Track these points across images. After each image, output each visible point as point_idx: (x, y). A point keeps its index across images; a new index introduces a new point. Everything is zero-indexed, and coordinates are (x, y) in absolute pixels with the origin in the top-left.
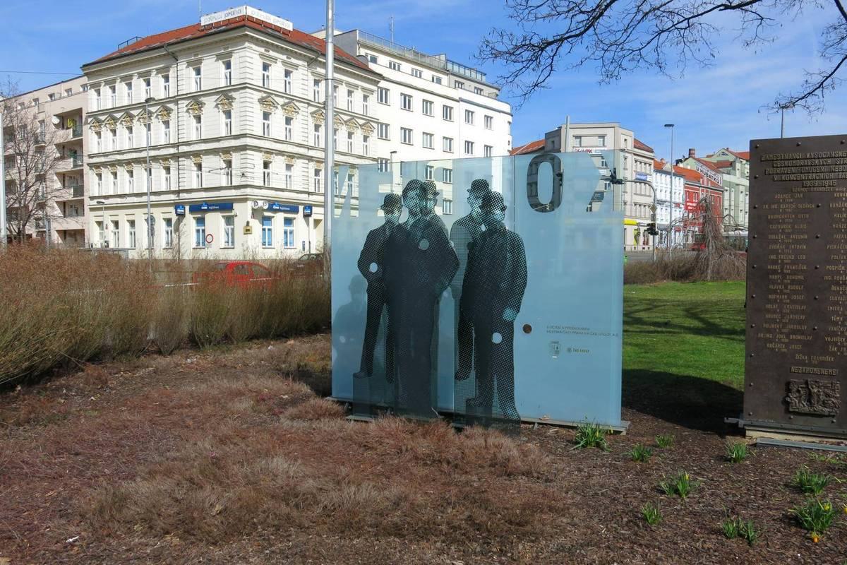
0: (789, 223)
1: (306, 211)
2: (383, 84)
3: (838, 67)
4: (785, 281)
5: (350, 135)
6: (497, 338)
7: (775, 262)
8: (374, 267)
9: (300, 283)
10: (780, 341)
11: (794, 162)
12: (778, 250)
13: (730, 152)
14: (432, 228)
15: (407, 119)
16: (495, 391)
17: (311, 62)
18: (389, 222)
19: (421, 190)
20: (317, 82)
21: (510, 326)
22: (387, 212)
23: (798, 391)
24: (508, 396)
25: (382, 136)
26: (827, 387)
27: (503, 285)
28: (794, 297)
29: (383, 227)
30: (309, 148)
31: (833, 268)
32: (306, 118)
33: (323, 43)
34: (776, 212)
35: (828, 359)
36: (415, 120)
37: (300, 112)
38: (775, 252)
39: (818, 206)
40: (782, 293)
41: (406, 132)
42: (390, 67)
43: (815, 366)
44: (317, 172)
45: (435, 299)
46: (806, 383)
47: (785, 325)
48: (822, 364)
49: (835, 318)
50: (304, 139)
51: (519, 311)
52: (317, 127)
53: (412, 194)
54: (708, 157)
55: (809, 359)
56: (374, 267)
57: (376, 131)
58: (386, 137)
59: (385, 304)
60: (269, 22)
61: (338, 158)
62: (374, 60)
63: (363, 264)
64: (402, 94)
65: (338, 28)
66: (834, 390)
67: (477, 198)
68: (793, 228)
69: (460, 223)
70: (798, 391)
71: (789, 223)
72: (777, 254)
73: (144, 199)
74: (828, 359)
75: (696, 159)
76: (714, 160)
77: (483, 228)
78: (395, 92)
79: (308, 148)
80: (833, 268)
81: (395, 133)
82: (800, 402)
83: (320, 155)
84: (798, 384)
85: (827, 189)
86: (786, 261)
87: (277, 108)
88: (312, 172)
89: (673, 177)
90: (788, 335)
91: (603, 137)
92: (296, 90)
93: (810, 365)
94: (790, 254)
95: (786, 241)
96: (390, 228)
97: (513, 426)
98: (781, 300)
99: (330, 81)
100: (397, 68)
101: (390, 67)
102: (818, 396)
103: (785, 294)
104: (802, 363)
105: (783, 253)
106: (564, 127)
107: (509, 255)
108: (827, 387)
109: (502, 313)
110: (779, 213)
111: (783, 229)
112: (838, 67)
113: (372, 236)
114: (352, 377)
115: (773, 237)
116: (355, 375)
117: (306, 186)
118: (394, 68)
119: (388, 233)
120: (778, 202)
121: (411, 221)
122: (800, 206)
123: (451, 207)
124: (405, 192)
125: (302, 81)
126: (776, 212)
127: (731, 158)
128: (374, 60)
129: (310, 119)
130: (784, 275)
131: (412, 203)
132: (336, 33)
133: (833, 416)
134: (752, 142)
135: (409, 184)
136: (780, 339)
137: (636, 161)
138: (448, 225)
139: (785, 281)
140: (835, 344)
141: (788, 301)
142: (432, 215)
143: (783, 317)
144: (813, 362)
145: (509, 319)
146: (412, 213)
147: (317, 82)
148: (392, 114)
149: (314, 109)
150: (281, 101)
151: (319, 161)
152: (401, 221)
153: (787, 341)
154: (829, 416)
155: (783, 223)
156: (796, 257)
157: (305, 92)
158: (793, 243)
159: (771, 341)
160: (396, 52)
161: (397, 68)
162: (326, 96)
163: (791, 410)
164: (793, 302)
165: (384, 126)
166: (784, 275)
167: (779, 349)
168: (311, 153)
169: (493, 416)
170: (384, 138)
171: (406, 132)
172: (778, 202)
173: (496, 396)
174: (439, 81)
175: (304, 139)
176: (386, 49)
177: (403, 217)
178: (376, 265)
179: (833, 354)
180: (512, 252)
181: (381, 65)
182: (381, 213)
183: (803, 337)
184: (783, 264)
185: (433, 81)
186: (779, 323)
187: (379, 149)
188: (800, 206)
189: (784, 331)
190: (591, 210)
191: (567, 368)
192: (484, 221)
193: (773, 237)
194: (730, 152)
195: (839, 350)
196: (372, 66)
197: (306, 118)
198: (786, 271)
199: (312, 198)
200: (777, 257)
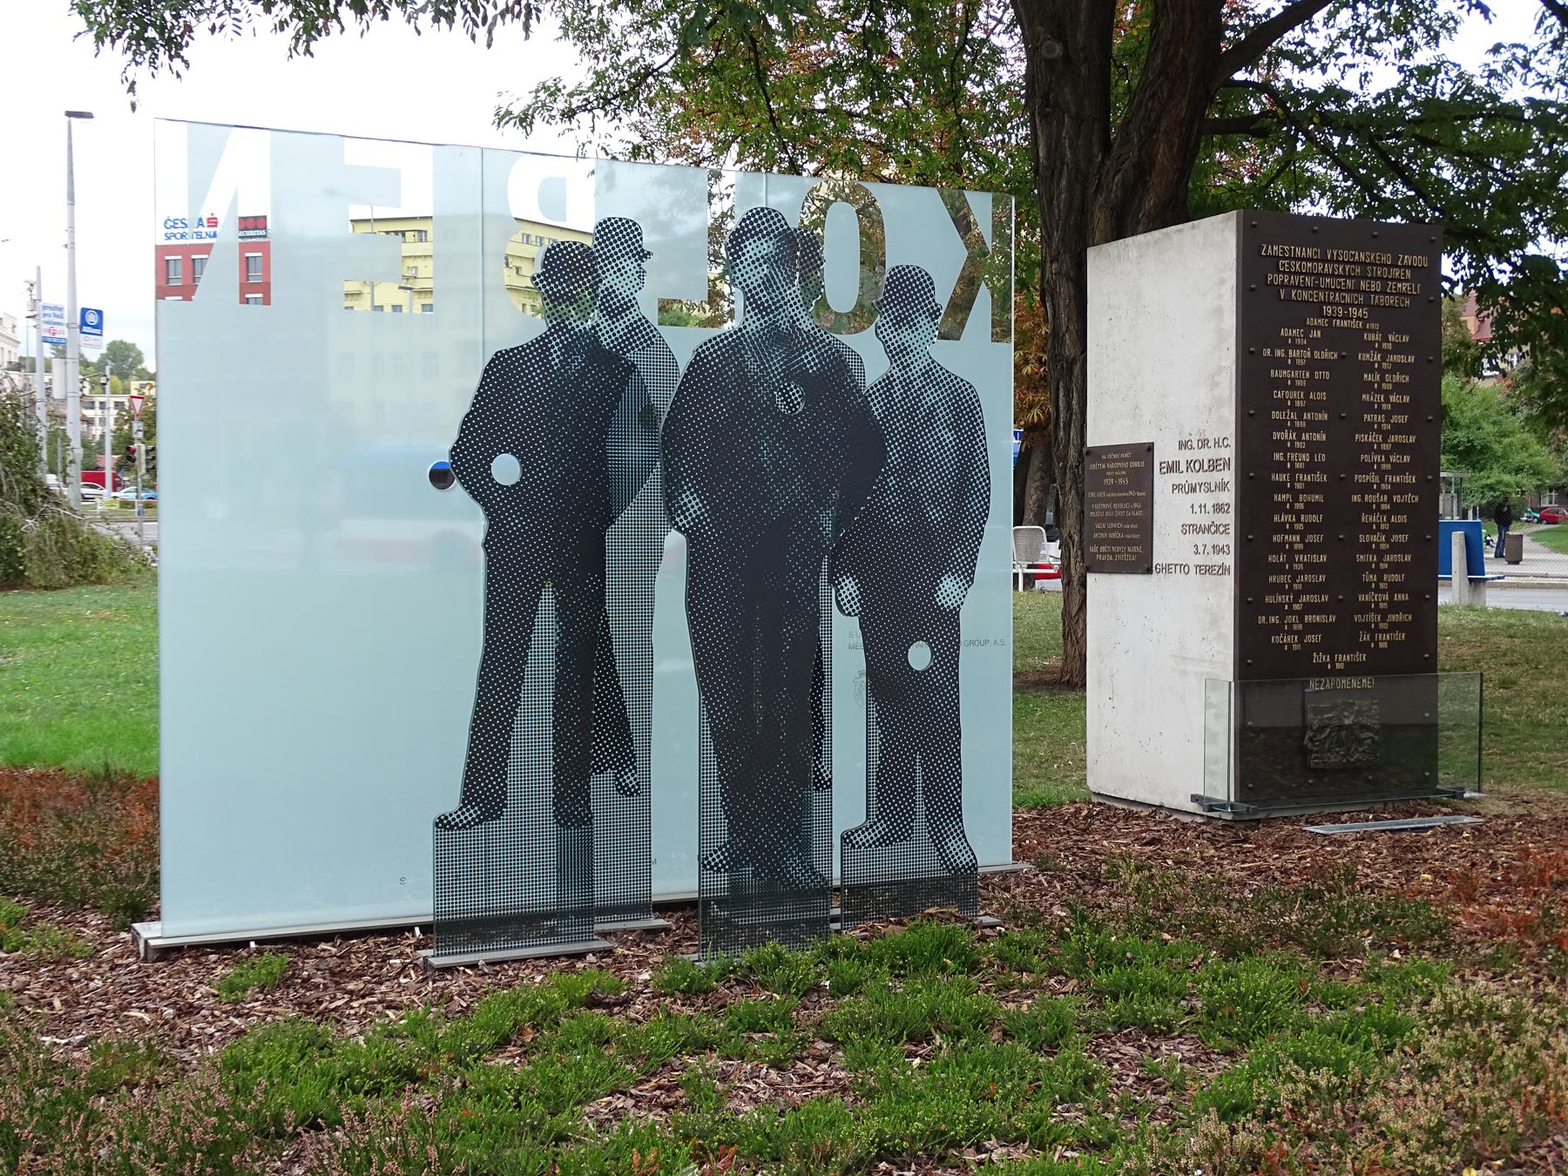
3: (71, 173)
8: (506, 470)
9: (515, 524)
10: (1291, 632)
12: (1285, 442)
28: (1310, 538)
34: (1281, 364)
38: (1281, 446)
56: (506, 470)
95: (1298, 424)
110: (1286, 367)
112: (71, 173)
113: (503, 372)
114: (429, 831)
116: (442, 824)
120: (1284, 344)
122: (1317, 355)
142: (631, 317)
145: (949, 603)
156: (1312, 457)
166: (1295, 494)
167: (1290, 645)
172: (1284, 344)
178: (508, 456)
179: (1364, 647)
180: (955, 427)
184: (1293, 471)
188: (1317, 355)
189: (1297, 607)
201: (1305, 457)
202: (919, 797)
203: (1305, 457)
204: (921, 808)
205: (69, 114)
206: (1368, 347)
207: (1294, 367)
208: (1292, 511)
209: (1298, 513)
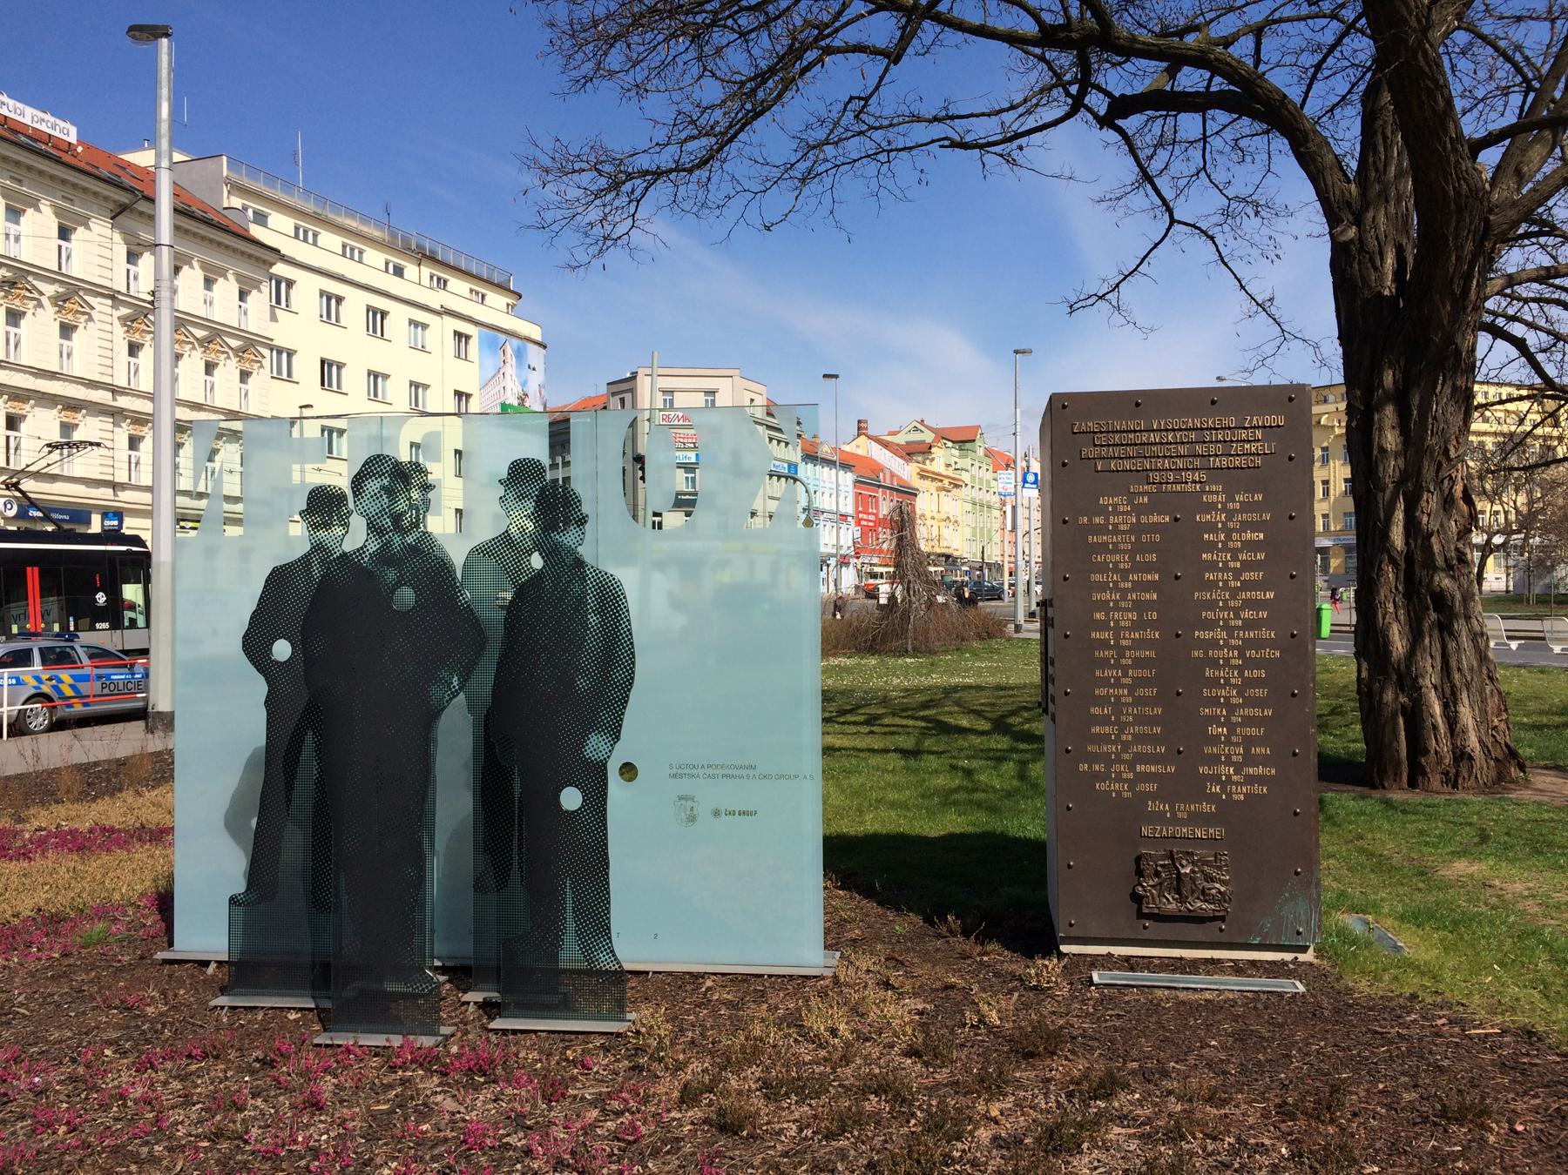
0: (1125, 552)
1: (107, 523)
2: (280, 269)
4: (1123, 661)
5: (210, 368)
6: (571, 799)
7: (1102, 626)
8: (282, 650)
10: (1119, 779)
11: (1131, 436)
13: (928, 428)
14: (427, 565)
15: (333, 343)
16: (569, 915)
17: (118, 213)
18: (318, 547)
19: (394, 479)
20: (132, 257)
21: (600, 769)
22: (314, 527)
23: (1157, 874)
24: (597, 923)
25: (279, 371)
26: (1207, 863)
27: (582, 683)
29: (305, 560)
30: (115, 391)
31: (1208, 635)
32: (108, 328)
33: (149, 176)
35: (1207, 807)
36: (353, 347)
37: (94, 313)
38: (1103, 606)
39: (1176, 520)
40: (1118, 684)
41: (328, 370)
42: (297, 237)
43: (1183, 823)
44: (134, 443)
45: (433, 714)
46: (1171, 856)
47: (1126, 746)
48: (1197, 819)
49: (1214, 730)
50: (103, 370)
51: (618, 738)
52: (134, 349)
53: (373, 486)
54: (891, 434)
55: (1172, 810)
56: (282, 650)
57: (266, 362)
58: (289, 374)
59: (310, 733)
60: (20, 119)
61: (184, 414)
62: (261, 219)
63: (255, 645)
64: (322, 293)
65: (183, 150)
66: (1220, 868)
67: (521, 497)
68: (1132, 559)
69: (482, 551)
70: (1157, 874)
71: (1125, 552)
72: (1107, 610)
73: (720, 772)
74: (1207, 807)
75: (869, 437)
76: (901, 439)
77: (537, 561)
78: (307, 289)
79: (113, 391)
80: (1208, 635)
81: (306, 368)
82: (1161, 895)
83: (145, 406)
84: (1155, 859)
85: (1190, 487)
86: (1122, 624)
87: (40, 305)
88: (124, 442)
89: (841, 473)
90: (1131, 765)
91: (713, 393)
92: (78, 268)
93: (1175, 821)
94: (1128, 610)
95: (1122, 585)
96: (322, 561)
97: (616, 986)
98: (1118, 697)
99: (165, 250)
100: (310, 240)
101: (297, 237)
102: (1193, 880)
103: (1124, 686)
104: (1159, 818)
105: (1117, 609)
106: (641, 372)
107: (593, 619)
108: (1207, 863)
109: (581, 744)
110: (1107, 532)
111: (1116, 564)
113: (279, 579)
115: (1098, 577)
116: (233, 901)
117: (110, 470)
118: (305, 240)
119: (316, 572)
120: (1103, 511)
121: (373, 547)
122: (1144, 519)
123: (463, 517)
124: (358, 482)
125: (97, 251)
126: (1102, 529)
127: (928, 437)
128: (261, 219)
129: (120, 331)
130: (1121, 651)
131: (374, 508)
132: (177, 157)
133: (1222, 919)
134: (1053, 399)
135: (366, 463)
136: (1119, 774)
137: (771, 439)
138: (457, 555)
139: (1123, 661)
140: (1216, 779)
141: (1130, 700)
143: (1121, 731)
144: (1180, 815)
146: (373, 528)
147: (132, 257)
148: (300, 329)
149: (124, 311)
150: (49, 289)
151: (139, 420)
152: (348, 547)
153: (1131, 776)
154: (1215, 919)
155: (1116, 551)
157: (108, 274)
158: (1133, 590)
159: (1104, 777)
160: (310, 207)
161: (310, 240)
162: (156, 280)
163: (1145, 911)
164: (1139, 701)
165: (284, 355)
166: (1121, 651)
167: (1119, 793)
168: (123, 402)
169: (562, 965)
170: (285, 376)
171: (328, 370)
172: (1103, 511)
173: (571, 925)
174: (399, 272)
175: (103, 370)
176: (285, 199)
177: (355, 536)
179: (1213, 798)
181: (277, 230)
182: (298, 530)
183: (1160, 769)
184: (1118, 629)
185: (387, 271)
186: (1114, 743)
187: (268, 396)
188: (1144, 519)
190: (660, 527)
191: (716, 857)
192: (538, 547)
193: (1098, 577)
194: (928, 428)
195: (1223, 790)
196: (256, 231)
197: (108, 328)
198: (1124, 643)
199: (125, 495)
200: (1107, 615)
201: (1133, 616)
202: (569, 915)
203: (1133, 616)
204: (571, 925)
205: (1016, 352)
206: (1211, 507)
207: (1116, 531)
208: (1117, 666)
209: (1125, 669)
